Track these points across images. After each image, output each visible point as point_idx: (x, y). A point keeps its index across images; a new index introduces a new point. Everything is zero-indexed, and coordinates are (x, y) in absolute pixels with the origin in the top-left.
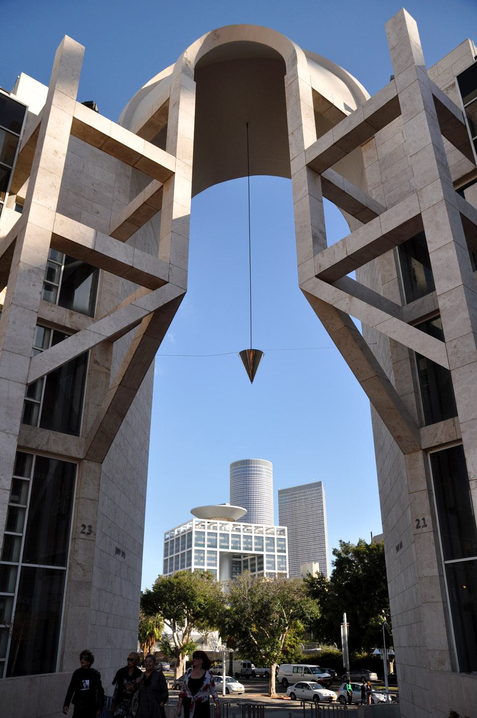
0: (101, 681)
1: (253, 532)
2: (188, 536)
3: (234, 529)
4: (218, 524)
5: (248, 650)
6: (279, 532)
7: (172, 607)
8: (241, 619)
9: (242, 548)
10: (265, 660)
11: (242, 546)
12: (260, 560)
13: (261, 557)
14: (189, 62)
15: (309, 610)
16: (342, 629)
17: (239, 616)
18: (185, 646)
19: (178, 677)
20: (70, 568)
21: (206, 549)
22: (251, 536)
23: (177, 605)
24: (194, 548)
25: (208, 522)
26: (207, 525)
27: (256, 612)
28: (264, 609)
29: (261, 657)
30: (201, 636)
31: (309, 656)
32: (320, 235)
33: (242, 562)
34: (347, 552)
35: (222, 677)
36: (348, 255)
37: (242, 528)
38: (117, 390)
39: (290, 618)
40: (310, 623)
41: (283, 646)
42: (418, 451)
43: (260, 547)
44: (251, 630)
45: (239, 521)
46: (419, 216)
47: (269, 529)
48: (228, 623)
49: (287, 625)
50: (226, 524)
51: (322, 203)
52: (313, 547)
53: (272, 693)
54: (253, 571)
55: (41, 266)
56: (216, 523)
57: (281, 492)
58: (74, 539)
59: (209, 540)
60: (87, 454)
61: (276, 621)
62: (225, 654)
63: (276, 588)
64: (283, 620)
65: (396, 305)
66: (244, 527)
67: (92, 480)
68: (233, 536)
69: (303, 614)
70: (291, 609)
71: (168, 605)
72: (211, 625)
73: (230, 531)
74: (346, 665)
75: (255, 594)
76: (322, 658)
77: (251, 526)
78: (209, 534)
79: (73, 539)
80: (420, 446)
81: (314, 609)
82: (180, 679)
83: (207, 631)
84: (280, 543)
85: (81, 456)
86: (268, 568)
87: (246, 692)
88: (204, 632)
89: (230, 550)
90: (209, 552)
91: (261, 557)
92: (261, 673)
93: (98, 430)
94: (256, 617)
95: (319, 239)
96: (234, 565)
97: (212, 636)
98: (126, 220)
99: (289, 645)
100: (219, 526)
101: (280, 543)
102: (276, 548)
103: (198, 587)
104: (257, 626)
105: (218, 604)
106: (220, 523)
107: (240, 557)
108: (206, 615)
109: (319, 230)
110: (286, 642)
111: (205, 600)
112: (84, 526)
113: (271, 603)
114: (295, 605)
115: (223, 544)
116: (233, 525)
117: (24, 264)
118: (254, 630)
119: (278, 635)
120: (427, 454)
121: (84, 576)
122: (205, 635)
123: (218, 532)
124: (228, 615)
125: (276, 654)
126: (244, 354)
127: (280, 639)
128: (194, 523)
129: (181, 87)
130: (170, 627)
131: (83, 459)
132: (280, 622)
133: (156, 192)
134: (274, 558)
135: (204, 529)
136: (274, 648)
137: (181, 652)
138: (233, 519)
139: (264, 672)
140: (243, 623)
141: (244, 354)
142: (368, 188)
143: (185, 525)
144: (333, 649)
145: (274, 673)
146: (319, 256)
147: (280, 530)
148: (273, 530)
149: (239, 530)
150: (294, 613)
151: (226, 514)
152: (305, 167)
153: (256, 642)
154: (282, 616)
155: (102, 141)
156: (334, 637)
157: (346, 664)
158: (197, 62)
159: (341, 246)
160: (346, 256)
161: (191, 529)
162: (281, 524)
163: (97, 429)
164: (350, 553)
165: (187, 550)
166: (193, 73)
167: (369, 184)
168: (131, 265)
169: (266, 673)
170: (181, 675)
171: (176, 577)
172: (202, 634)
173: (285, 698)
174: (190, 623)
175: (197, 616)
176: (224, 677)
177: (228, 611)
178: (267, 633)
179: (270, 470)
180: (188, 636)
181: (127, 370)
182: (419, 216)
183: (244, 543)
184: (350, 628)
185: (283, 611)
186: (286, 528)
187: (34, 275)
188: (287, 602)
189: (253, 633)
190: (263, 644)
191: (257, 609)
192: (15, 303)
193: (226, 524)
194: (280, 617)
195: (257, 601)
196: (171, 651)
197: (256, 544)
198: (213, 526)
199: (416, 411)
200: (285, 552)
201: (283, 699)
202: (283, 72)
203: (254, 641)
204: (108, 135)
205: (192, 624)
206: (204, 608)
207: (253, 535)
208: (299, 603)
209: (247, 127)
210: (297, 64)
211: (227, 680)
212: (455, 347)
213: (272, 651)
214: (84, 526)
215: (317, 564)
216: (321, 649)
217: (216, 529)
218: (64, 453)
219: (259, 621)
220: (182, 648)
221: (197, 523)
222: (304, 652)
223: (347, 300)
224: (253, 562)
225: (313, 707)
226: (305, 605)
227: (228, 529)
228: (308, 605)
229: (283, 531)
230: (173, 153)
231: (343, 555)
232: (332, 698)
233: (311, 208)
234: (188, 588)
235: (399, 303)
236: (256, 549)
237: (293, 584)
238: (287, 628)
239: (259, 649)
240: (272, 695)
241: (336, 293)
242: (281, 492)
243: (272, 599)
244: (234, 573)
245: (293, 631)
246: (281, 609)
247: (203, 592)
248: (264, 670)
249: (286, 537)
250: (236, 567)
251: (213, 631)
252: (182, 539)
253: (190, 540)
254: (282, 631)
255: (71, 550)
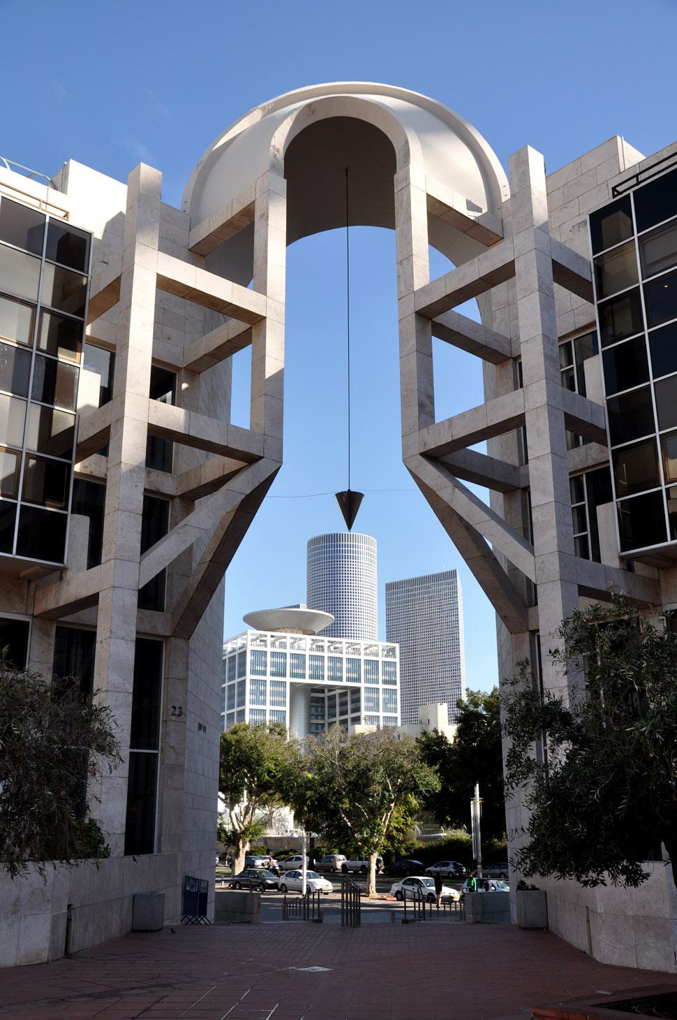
0: (285, 178)
1: (345, 651)
2: (239, 658)
3: (314, 646)
4: (288, 638)
5: (337, 835)
6: (385, 653)
7: (229, 775)
8: (328, 793)
9: (326, 677)
10: (362, 848)
11: (326, 674)
12: (355, 697)
13: (356, 691)
14: (278, 150)
15: (424, 780)
16: (472, 806)
17: (326, 788)
18: (247, 829)
19: (237, 873)
20: (162, 751)
21: (269, 678)
22: (341, 659)
23: (236, 772)
24: (249, 677)
25: (272, 636)
26: (269, 640)
27: (349, 783)
28: (361, 778)
29: (356, 844)
30: (263, 815)
31: (426, 843)
32: (427, 402)
33: (326, 700)
34: (476, 705)
35: (301, 871)
36: (454, 439)
37: (326, 645)
38: (208, 566)
39: (398, 791)
40: (425, 798)
41: (388, 829)
42: (525, 632)
43: (355, 676)
44: (342, 808)
45: (322, 633)
46: (523, 414)
47: (371, 646)
48: (310, 797)
49: (392, 801)
50: (301, 639)
51: (432, 357)
52: (440, 675)
53: (371, 892)
54: (343, 713)
55: (141, 463)
56: (285, 637)
57: (390, 587)
58: (164, 721)
59: (273, 664)
60: (175, 631)
61: (378, 795)
62: (305, 840)
63: (378, 750)
64: (387, 794)
65: (512, 466)
66: (330, 644)
67: (180, 658)
68: (313, 658)
69: (416, 786)
70: (399, 778)
71: (224, 772)
72: (286, 800)
73: (307, 649)
74: (477, 856)
75: (348, 758)
76: (445, 846)
77: (341, 643)
78: (274, 654)
79: (163, 721)
80: (527, 627)
81: (431, 779)
82: (240, 875)
83: (272, 806)
84: (387, 669)
85: (168, 634)
86: (368, 709)
87: (334, 891)
88: (267, 809)
89: (307, 681)
90: (274, 683)
91: (356, 691)
92: (356, 867)
93: (187, 606)
94: (350, 790)
95: (425, 406)
96: (312, 704)
97: (280, 815)
98: (205, 355)
99: (395, 828)
100: (289, 641)
101: (387, 669)
102: (381, 678)
103: (266, 747)
104: (350, 802)
105: (297, 771)
106: (291, 638)
107: (323, 691)
108: (279, 788)
109: (425, 395)
110: (392, 824)
111: (276, 765)
112: (174, 707)
113: (370, 771)
114: (405, 774)
115: (295, 671)
116: (312, 640)
117: (126, 464)
118: (346, 805)
119: (380, 815)
120: (534, 637)
121: (177, 759)
122: (269, 812)
123: (288, 651)
124: (310, 787)
125: (377, 839)
126: (340, 496)
127: (383, 820)
128: (250, 637)
129: (270, 193)
130: (225, 802)
131: (170, 637)
132: (383, 796)
133: (244, 332)
134: (378, 693)
135: (266, 646)
136: (374, 832)
137: (241, 837)
138: (312, 631)
139: (360, 865)
140: (332, 798)
141: (340, 496)
142: (493, 306)
143: (236, 641)
144: (461, 834)
145: (374, 867)
146: (424, 431)
147: (388, 648)
148: (376, 648)
149: (321, 648)
150: (403, 785)
151: (302, 624)
152: (414, 315)
153: (349, 824)
154: (386, 788)
155: (187, 292)
156: (462, 818)
157: (477, 855)
158: (287, 147)
159: (446, 425)
160: (451, 440)
161: (244, 646)
162: (389, 639)
163: (185, 606)
164: (480, 705)
165: (237, 680)
166: (283, 166)
167: (494, 301)
168: (226, 445)
169: (363, 867)
170: (242, 870)
171: (235, 732)
172: (265, 812)
173: (387, 899)
174: (254, 797)
175: (263, 787)
176: (305, 871)
177: (309, 781)
178: (365, 811)
179: (374, 552)
180: (252, 815)
181: (219, 545)
182: (523, 414)
183: (330, 669)
184: (483, 806)
185: (388, 781)
186: (397, 646)
187: (135, 475)
188: (393, 769)
189: (345, 812)
190: (359, 827)
191: (352, 778)
192: (121, 508)
193: (301, 639)
194: (383, 790)
195: (351, 768)
196: (227, 836)
197: (349, 671)
198: (280, 643)
199: (525, 589)
200: (394, 683)
201: (385, 899)
202: (392, 169)
203: (346, 823)
204: (194, 287)
205: (257, 799)
206: (275, 776)
207: (344, 656)
208: (410, 771)
209: (347, 175)
210: (409, 163)
211: (308, 875)
212: (542, 562)
213: (372, 836)
214: (174, 707)
215: (445, 705)
216: (445, 834)
217: (285, 647)
218: (150, 631)
219: (354, 795)
220: (243, 833)
221: (254, 637)
222: (418, 839)
223: (450, 490)
224: (344, 699)
225: (426, 909)
226: (418, 773)
227: (303, 647)
228: (422, 774)
229: (393, 650)
230: (262, 289)
231: (471, 708)
232: (452, 898)
233: (419, 369)
234: (251, 748)
235: (517, 465)
236: (349, 679)
237: (403, 744)
238: (392, 805)
239: (353, 833)
240: (370, 895)
241: (440, 479)
242: (390, 587)
243: (372, 765)
244: (312, 717)
245: (403, 809)
246: (385, 778)
247: (274, 755)
248: (359, 863)
249: (397, 660)
250: (317, 707)
251: (281, 806)
252: (230, 662)
253: (243, 664)
254: (386, 809)
255: (162, 733)
